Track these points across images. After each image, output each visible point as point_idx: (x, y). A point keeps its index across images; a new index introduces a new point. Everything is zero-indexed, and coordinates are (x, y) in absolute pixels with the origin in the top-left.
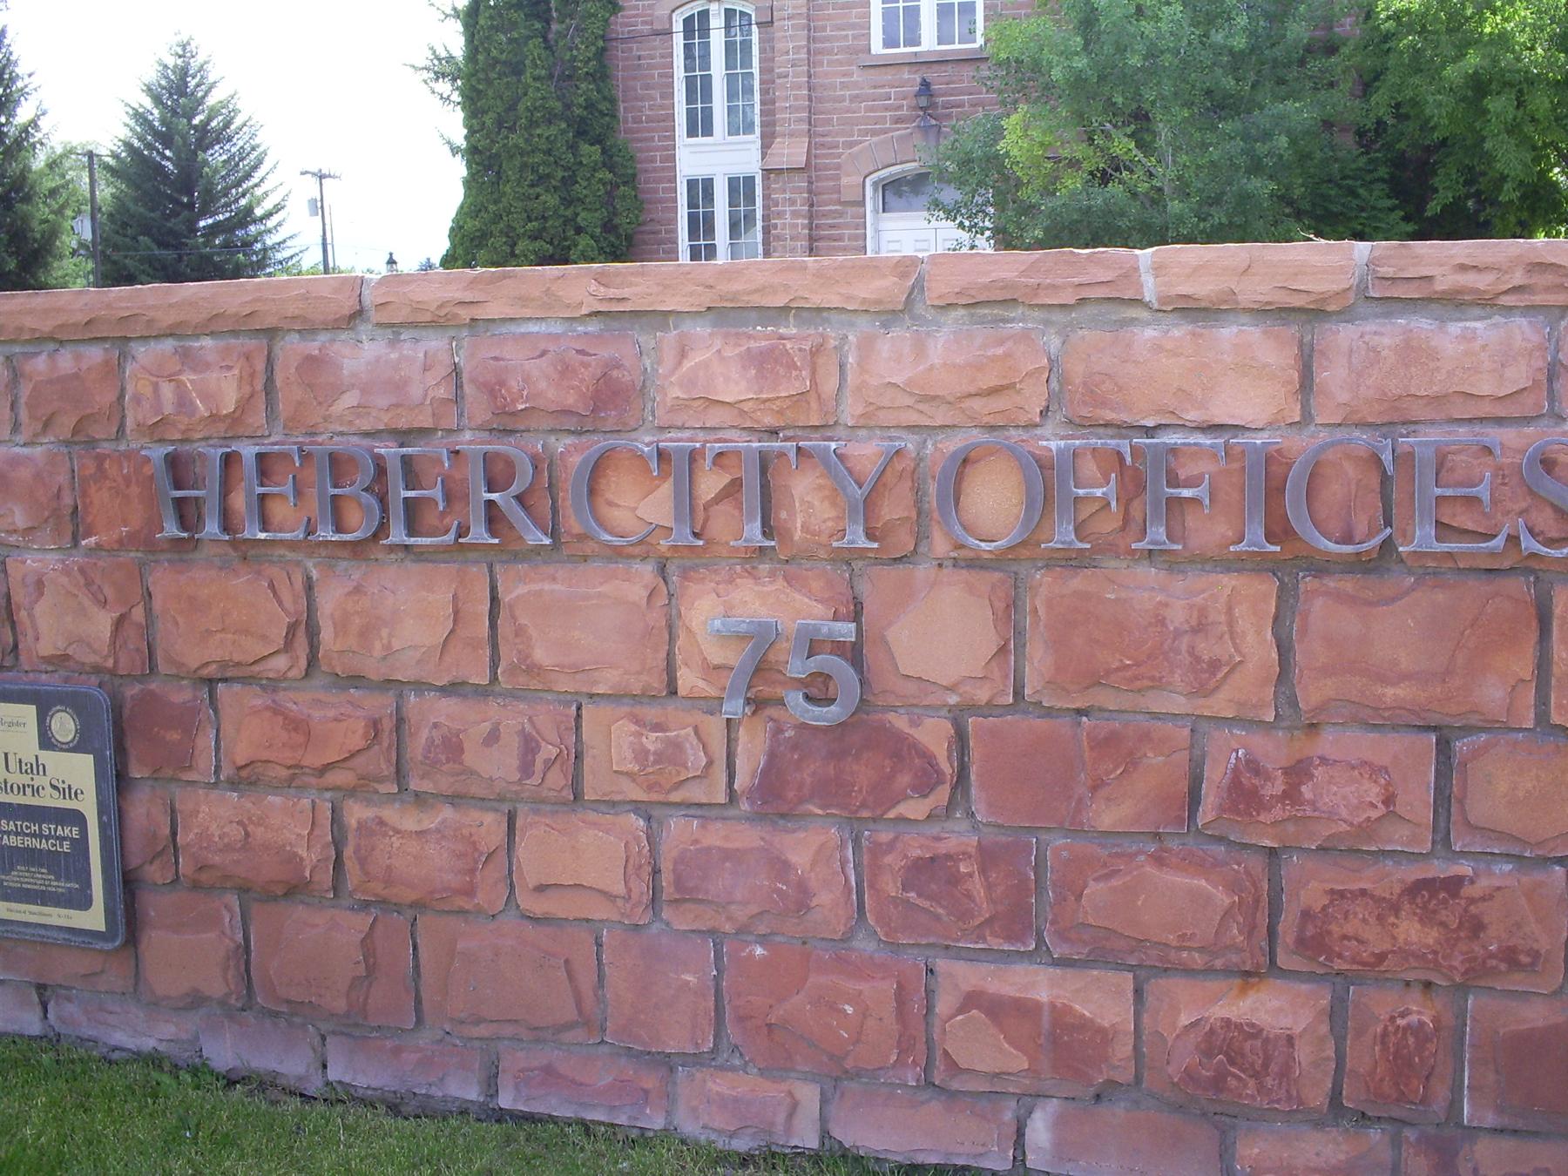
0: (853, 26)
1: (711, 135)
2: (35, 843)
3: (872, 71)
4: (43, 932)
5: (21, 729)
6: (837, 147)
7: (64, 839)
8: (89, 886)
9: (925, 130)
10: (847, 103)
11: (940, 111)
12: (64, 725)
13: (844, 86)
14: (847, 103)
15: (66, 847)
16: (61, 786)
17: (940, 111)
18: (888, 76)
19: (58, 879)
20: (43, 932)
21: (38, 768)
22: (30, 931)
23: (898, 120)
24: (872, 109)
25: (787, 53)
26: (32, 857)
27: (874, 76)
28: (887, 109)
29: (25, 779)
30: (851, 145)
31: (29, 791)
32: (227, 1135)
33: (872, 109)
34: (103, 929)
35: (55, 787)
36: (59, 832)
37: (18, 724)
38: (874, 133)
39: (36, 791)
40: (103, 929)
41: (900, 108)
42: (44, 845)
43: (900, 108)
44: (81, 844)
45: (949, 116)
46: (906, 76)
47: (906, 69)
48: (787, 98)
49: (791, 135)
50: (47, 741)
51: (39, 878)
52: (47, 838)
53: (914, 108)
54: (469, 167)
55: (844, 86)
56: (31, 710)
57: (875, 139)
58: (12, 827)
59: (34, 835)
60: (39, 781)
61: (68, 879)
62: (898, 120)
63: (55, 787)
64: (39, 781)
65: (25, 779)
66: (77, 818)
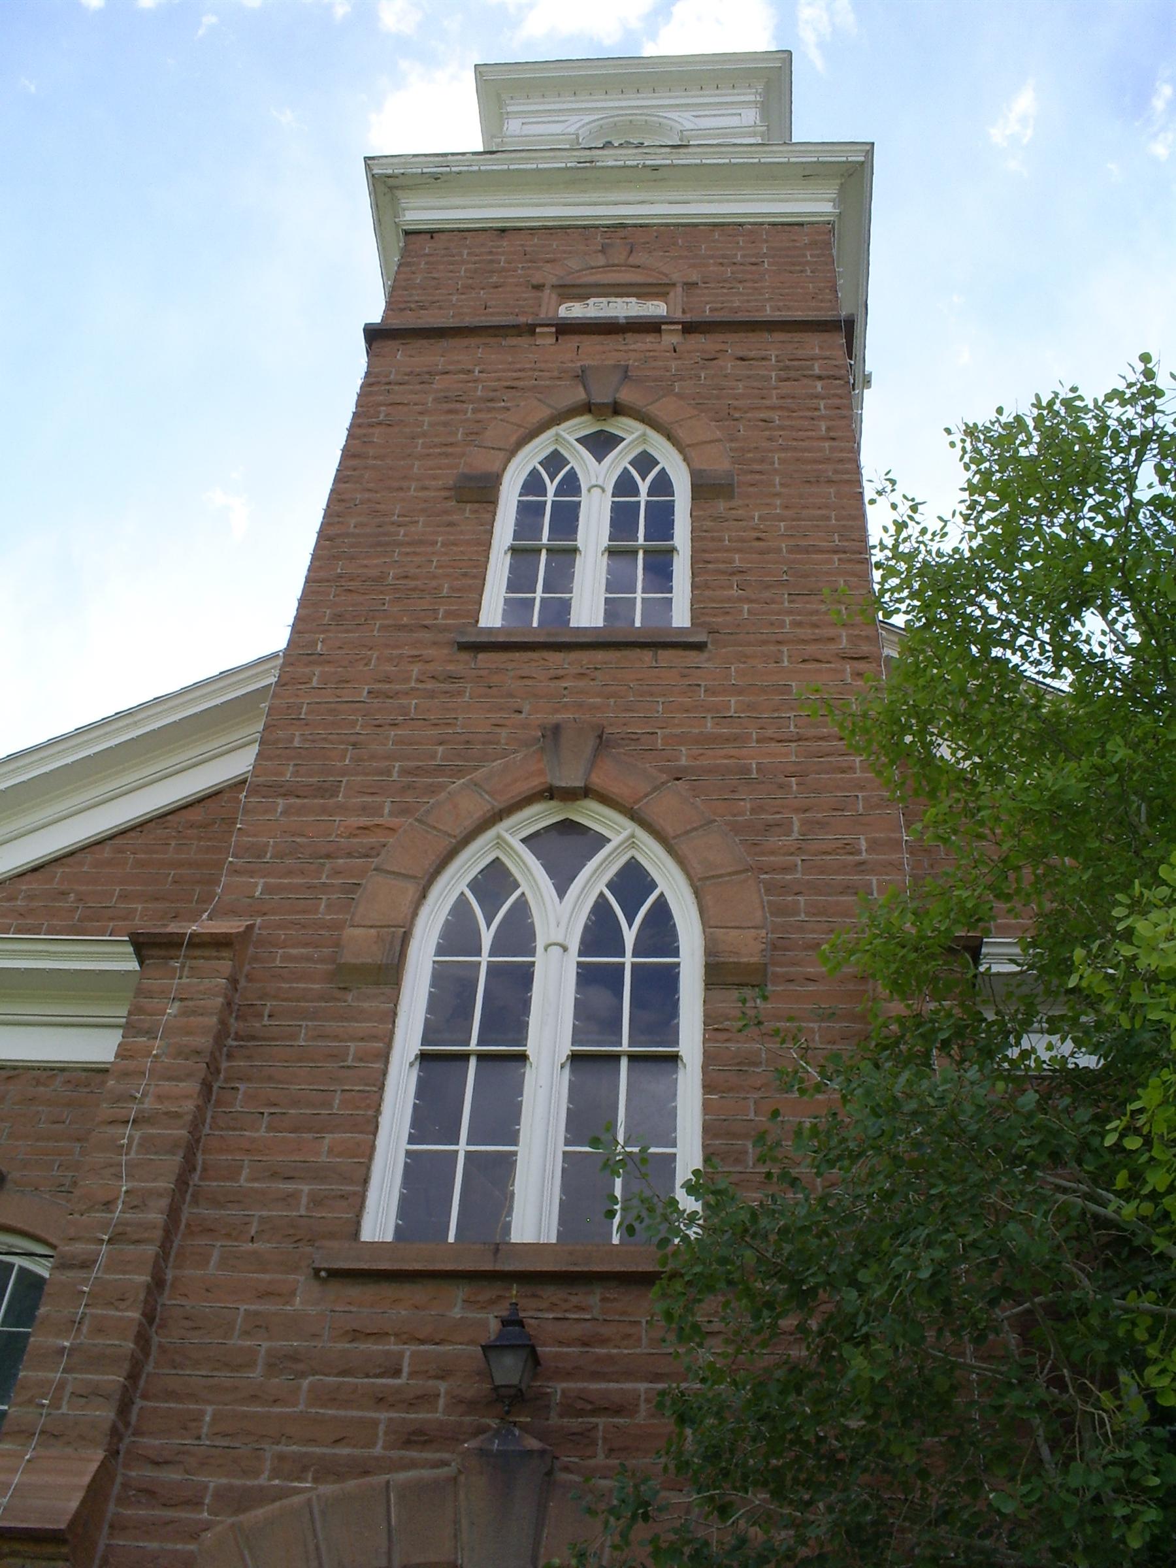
0: (317, 1174)
1: (497, 858)
3: (354, 1291)
6: (195, 1503)
9: (502, 1466)
10: (257, 1374)
11: (554, 1420)
13: (258, 1325)
14: (257, 1374)
17: (554, 1420)
18: (400, 1307)
23: (416, 1438)
24: (332, 1398)
25: (108, 1205)
27: (363, 1305)
28: (380, 1401)
30: (242, 1501)
32: (720, 1394)
33: (332, 1398)
34: (482, 624)
38: (328, 1471)
40: (482, 624)
41: (426, 1399)
43: (426, 1399)
45: (584, 1438)
46: (457, 1313)
47: (461, 1292)
48: (75, 1324)
49: (51, 1436)
53: (471, 1405)
55: (258, 1325)
57: (328, 1489)
62: (416, 1438)
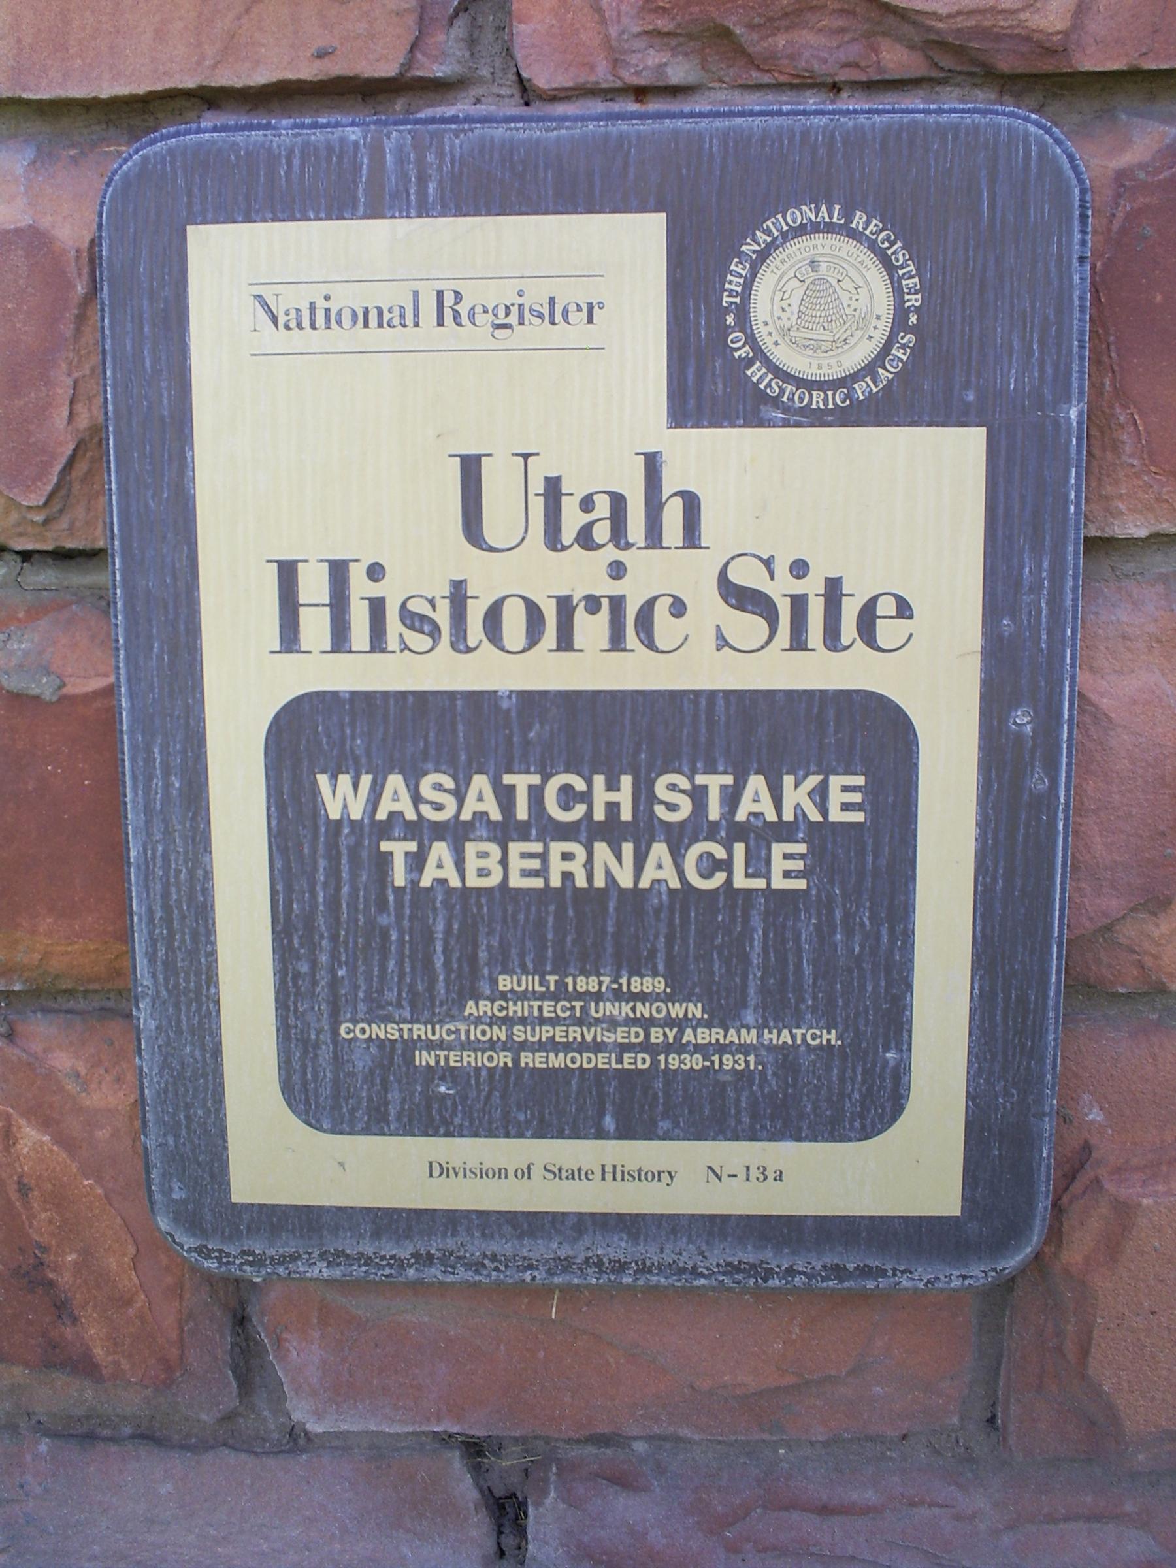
2: (614, 866)
4: (618, 1248)
5: (575, 331)
7: (783, 831)
8: (894, 1022)
12: (827, 296)
15: (785, 866)
16: (780, 589)
19: (721, 1016)
20: (618, 1248)
21: (664, 509)
22: (541, 1249)
26: (581, 931)
29: (582, 573)
31: (591, 629)
35: (741, 598)
36: (756, 798)
37: (552, 313)
39: (631, 624)
42: (660, 867)
44: (871, 866)
50: (713, 379)
51: (627, 1018)
52: (678, 838)
54: (602, 841)
56: (632, 247)
58: (481, 800)
59: (610, 830)
60: (649, 575)
61: (778, 1010)
63: (741, 598)
64: (649, 575)
65: (582, 573)
66: (874, 736)
